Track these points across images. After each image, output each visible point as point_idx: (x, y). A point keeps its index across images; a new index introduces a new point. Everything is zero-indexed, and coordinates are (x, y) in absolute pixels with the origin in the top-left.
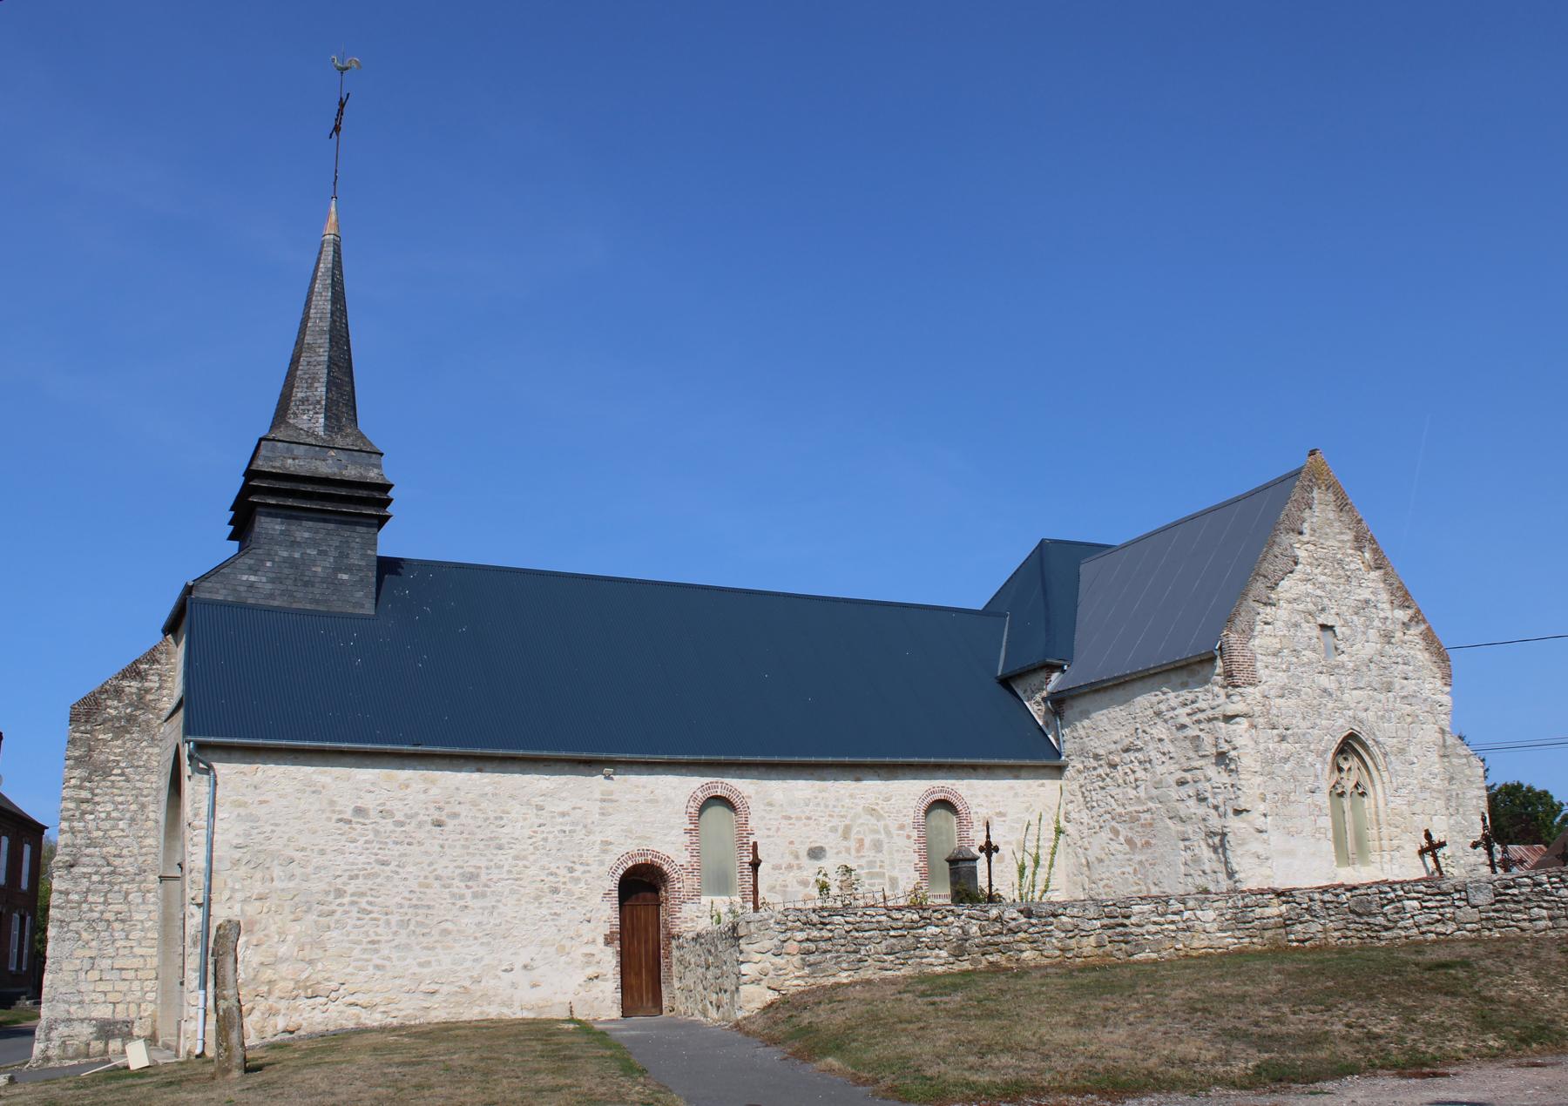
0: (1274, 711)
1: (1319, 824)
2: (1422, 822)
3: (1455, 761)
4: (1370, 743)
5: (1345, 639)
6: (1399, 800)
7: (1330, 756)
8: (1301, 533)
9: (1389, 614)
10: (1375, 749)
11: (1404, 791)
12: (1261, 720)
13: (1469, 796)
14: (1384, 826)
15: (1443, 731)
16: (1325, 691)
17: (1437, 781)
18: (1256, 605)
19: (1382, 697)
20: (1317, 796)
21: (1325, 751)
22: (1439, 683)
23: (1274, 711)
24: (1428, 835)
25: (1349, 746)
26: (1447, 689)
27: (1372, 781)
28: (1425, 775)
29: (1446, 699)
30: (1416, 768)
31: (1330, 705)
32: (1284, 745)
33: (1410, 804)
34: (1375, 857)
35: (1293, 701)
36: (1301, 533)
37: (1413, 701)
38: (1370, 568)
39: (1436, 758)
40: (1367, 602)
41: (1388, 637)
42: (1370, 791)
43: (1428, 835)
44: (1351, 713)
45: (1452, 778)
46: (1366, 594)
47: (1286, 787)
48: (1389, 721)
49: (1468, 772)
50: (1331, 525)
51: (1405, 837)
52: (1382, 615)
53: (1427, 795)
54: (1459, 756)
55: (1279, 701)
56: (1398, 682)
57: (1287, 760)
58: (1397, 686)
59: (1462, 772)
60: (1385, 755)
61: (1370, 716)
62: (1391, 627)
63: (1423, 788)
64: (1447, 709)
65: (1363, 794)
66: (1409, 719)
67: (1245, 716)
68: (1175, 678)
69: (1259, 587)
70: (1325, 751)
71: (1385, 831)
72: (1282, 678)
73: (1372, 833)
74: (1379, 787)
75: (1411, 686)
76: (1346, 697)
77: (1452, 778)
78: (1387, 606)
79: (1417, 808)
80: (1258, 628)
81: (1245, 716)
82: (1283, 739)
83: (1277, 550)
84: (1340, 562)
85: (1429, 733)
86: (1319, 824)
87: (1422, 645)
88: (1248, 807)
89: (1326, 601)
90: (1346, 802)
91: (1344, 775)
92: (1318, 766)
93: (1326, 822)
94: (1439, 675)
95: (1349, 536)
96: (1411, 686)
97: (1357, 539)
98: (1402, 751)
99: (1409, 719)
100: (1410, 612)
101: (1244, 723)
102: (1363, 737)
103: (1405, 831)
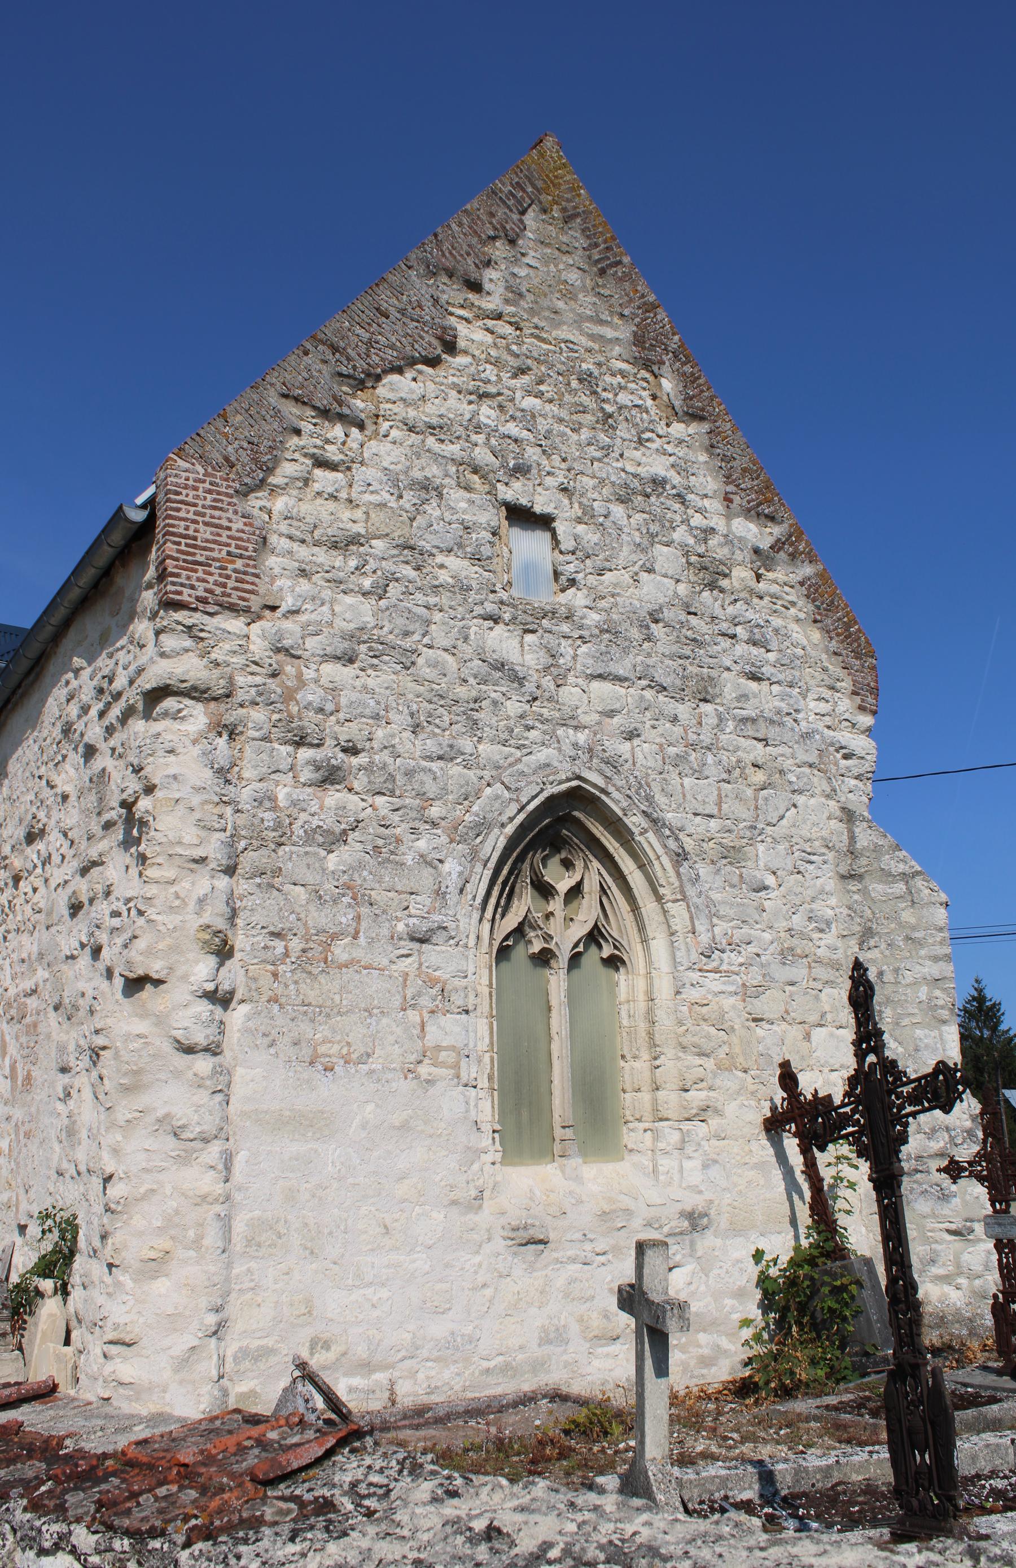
0: (311, 695)
1: (434, 1035)
2: (778, 1042)
3: (877, 888)
4: (634, 822)
5: (581, 552)
6: (713, 983)
7: (495, 842)
8: (476, 287)
9: (718, 522)
10: (650, 842)
11: (731, 959)
12: (258, 715)
13: (909, 977)
14: (670, 1051)
15: (849, 816)
16: (500, 666)
17: (830, 938)
18: (290, 409)
19: (683, 710)
20: (438, 957)
21: (482, 827)
22: (845, 705)
23: (311, 695)
24: (788, 1078)
25: (562, 827)
26: (866, 720)
27: (641, 928)
28: (798, 921)
29: (862, 744)
30: (772, 901)
31: (513, 707)
32: (334, 797)
33: (746, 993)
34: (633, 1136)
35: (383, 678)
36: (476, 287)
37: (773, 732)
38: (673, 414)
39: (828, 882)
40: (659, 483)
41: (711, 575)
42: (635, 954)
43: (788, 1078)
44: (582, 737)
45: (867, 933)
46: (659, 467)
47: (319, 918)
48: (699, 774)
49: (908, 916)
50: (569, 295)
51: (729, 1081)
52: (697, 520)
53: (799, 972)
54: (888, 876)
55: (331, 670)
56: (731, 685)
57: (335, 840)
58: (729, 693)
59: (894, 917)
60: (680, 857)
61: (644, 754)
62: (722, 553)
63: (787, 955)
64: (868, 766)
65: (614, 962)
66: (759, 777)
67: (197, 693)
68: (90, 625)
69: (311, 368)
70: (482, 827)
71: (670, 1066)
72: (355, 611)
73: (635, 1069)
74: (659, 945)
75: (766, 698)
76: (570, 694)
77: (867, 933)
78: (714, 505)
79: (769, 1004)
80: (287, 470)
81: (197, 693)
82: (330, 777)
83: (385, 298)
84: (586, 379)
85: (815, 817)
86: (434, 1035)
87: (804, 608)
88: (156, 968)
89: (532, 454)
90: (557, 981)
91: (556, 905)
92: (452, 867)
93: (478, 1033)
94: (846, 685)
95: (624, 332)
96: (766, 698)
97: (638, 340)
98: (732, 855)
99: (759, 777)
100: (777, 531)
101: (198, 717)
102: (616, 802)
103: (727, 1066)
